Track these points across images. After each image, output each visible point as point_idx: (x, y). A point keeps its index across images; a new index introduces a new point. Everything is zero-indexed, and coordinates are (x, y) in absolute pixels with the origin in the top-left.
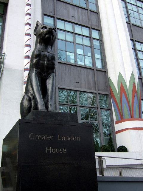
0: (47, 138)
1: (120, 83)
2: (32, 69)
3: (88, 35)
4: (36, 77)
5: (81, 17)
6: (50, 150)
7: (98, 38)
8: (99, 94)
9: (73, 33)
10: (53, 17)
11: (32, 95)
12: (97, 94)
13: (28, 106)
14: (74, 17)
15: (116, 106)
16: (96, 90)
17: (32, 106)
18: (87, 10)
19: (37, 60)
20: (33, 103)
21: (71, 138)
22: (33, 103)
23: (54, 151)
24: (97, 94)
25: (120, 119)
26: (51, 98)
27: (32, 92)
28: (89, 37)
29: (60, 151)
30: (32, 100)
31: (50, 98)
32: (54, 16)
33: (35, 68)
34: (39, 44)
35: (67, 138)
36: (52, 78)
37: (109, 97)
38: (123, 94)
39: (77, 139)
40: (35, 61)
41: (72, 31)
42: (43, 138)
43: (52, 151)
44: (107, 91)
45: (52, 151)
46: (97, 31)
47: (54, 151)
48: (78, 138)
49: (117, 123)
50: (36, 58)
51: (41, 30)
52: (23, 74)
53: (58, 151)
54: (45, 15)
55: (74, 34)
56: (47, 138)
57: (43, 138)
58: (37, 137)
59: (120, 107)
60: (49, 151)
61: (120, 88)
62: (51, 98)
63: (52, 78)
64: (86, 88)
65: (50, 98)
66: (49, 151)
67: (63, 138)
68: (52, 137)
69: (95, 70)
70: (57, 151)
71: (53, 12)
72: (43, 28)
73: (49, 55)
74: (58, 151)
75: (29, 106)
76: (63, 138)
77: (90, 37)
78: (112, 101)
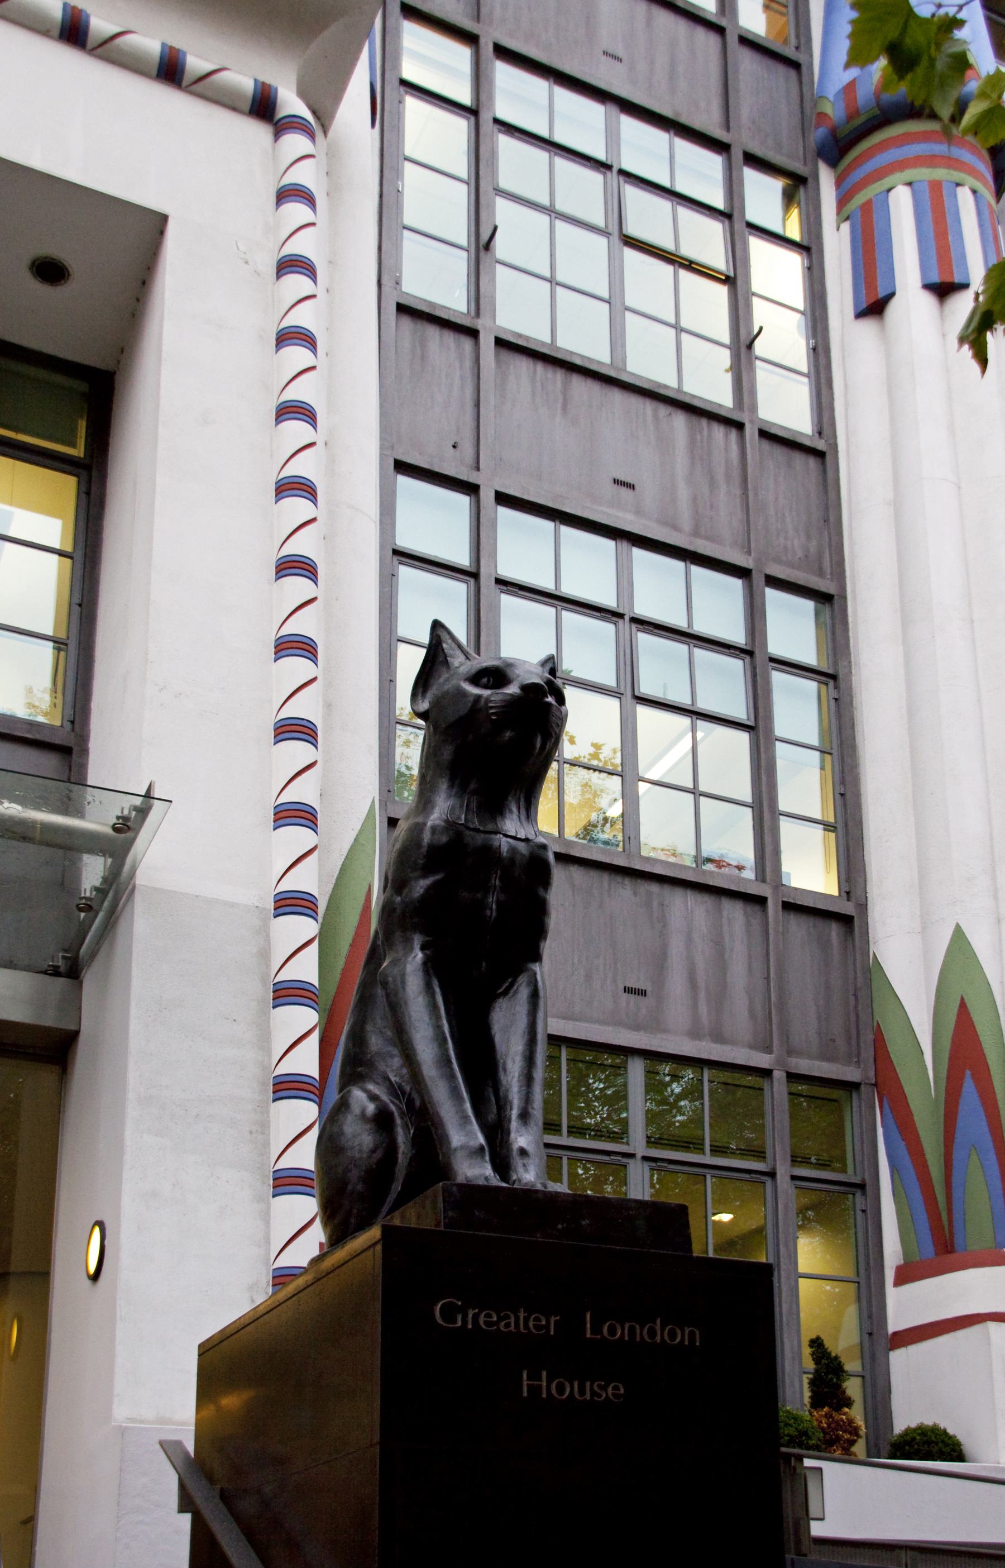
0: (526, 1326)
1: (959, 999)
2: (398, 934)
3: (738, 637)
4: (428, 987)
5: (683, 493)
6: (544, 1384)
7: (809, 657)
8: (793, 1077)
9: (621, 616)
10: (471, 489)
11: (394, 1090)
12: (779, 1075)
13: (373, 1151)
14: (631, 486)
15: (907, 1161)
16: (768, 1049)
17: (400, 1156)
18: (740, 426)
19: (429, 889)
20: (402, 1138)
21: (652, 1333)
22: (402, 1138)
23: (561, 1389)
24: (779, 1075)
25: (929, 1250)
26: (525, 1116)
27: (393, 1068)
28: (745, 653)
29: (593, 1393)
30: (398, 1121)
31: (515, 1113)
32: (472, 478)
33: (424, 932)
34: (451, 786)
35: (632, 1330)
36: (523, 993)
37: (863, 1096)
38: (969, 1087)
39: (682, 1336)
40: (421, 886)
41: (609, 601)
42: (508, 1325)
43: (554, 1391)
44: (854, 1057)
45: (554, 1391)
46: (808, 605)
47: (561, 1389)
48: (692, 1334)
49: (905, 1276)
50: (426, 871)
51: (474, 690)
52: (264, 933)
53: (582, 1392)
54: (402, 467)
55: (625, 625)
56: (526, 1326)
57: (508, 1325)
58: (476, 1317)
59: (936, 1171)
60: (535, 1390)
61: (947, 1044)
62: (525, 1116)
63: (523, 993)
64: (695, 1034)
65: (515, 1113)
66: (535, 1390)
67: (612, 1331)
68: (553, 1320)
69: (773, 907)
70: (579, 1392)
71: (467, 449)
72: (485, 680)
73: (513, 850)
74: (582, 1392)
75: (379, 1154)
76: (612, 1331)
77: (750, 653)
78: (880, 1131)
